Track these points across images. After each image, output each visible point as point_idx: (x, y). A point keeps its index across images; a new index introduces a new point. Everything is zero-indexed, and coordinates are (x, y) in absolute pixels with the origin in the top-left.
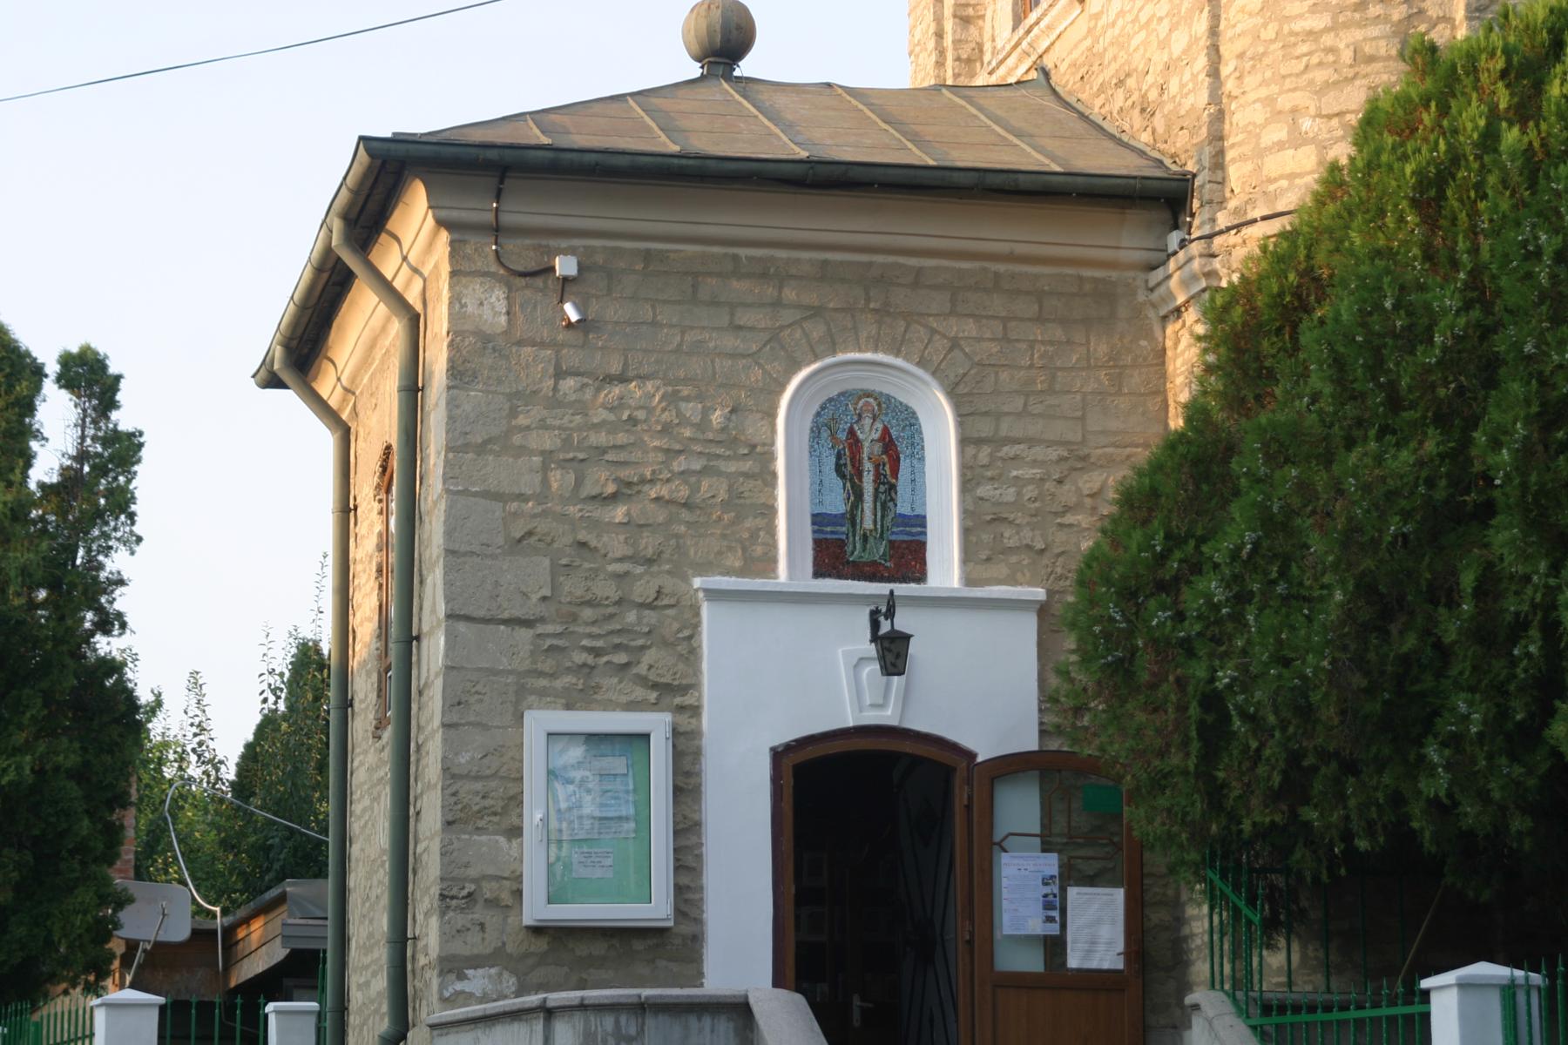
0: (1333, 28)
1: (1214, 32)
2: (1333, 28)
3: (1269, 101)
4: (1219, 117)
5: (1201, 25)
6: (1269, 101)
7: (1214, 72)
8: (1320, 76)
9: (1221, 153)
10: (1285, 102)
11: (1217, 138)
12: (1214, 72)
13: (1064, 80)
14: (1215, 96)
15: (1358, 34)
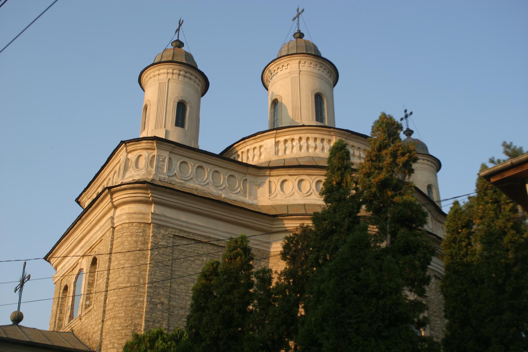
0: (122, 329)
1: (102, 328)
2: (122, 329)
3: (110, 340)
4: (101, 342)
5: (100, 326)
6: (110, 340)
7: (101, 334)
8: (119, 337)
9: (100, 348)
10: (112, 341)
11: (100, 346)
12: (101, 334)
13: (76, 332)
14: (101, 338)
15: (126, 331)
